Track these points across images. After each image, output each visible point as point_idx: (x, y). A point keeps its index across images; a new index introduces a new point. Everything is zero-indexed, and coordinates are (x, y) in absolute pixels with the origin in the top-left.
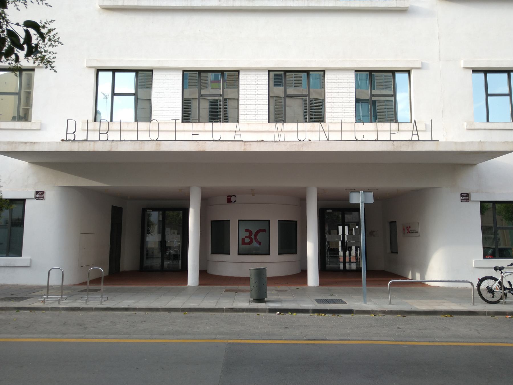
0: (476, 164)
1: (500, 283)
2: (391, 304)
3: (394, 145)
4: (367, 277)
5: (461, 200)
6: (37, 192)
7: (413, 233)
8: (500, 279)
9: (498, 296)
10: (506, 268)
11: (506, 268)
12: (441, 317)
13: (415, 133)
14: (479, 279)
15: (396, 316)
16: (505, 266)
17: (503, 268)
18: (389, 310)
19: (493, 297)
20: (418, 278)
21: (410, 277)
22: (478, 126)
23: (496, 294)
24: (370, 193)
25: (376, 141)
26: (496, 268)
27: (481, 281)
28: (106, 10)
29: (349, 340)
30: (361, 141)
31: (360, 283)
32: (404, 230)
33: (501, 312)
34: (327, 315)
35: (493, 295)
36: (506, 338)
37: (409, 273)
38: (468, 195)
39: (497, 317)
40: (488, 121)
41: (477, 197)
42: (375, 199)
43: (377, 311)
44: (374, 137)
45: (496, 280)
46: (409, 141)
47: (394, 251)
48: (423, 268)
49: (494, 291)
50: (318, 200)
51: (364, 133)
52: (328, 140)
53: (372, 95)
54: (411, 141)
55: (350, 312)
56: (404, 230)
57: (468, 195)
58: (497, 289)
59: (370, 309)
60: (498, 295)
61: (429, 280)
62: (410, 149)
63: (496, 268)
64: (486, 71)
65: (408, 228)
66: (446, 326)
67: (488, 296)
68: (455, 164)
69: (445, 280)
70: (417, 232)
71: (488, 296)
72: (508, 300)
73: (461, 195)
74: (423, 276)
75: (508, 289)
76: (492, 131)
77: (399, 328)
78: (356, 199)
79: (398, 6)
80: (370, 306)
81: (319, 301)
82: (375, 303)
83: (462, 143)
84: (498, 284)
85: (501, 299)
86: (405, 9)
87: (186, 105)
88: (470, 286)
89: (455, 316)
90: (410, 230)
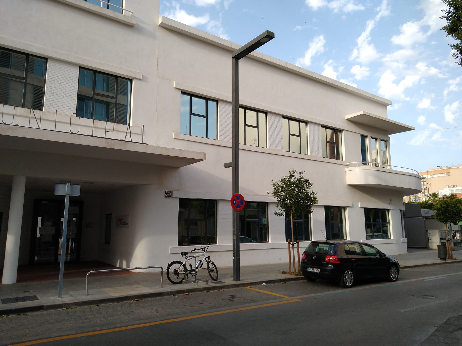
0: (179, 168)
1: (184, 266)
2: (88, 295)
3: (108, 143)
4: (65, 269)
5: (165, 196)
6: (166, 191)
7: (124, 224)
8: (184, 263)
9: (181, 276)
10: (190, 253)
11: (190, 253)
12: (132, 301)
13: (129, 134)
14: (169, 264)
15: (89, 307)
16: (189, 251)
17: (187, 253)
18: (83, 301)
19: (178, 278)
20: (124, 267)
21: (118, 265)
22: (182, 137)
23: (180, 275)
24: (78, 186)
25: (91, 136)
26: (182, 254)
27: (170, 265)
28: (163, 29)
29: (62, 336)
30: (76, 134)
31: (57, 276)
32: (117, 222)
33: (180, 291)
34: (11, 316)
35: (178, 276)
36: (177, 313)
37: (117, 261)
38: (171, 192)
39: (177, 295)
40: (190, 135)
41: (178, 195)
42: (82, 192)
43: (69, 304)
44: (96, 132)
45: (181, 263)
46: (123, 140)
47: (108, 242)
48: (128, 256)
49: (179, 273)
50: (26, 190)
51: (79, 127)
52: (39, 128)
53: (95, 93)
54: (125, 141)
55: (40, 308)
56: (117, 222)
57: (171, 192)
58: (181, 271)
59: (63, 303)
60: (181, 276)
61: (134, 267)
62: (122, 148)
63: (182, 254)
64: (192, 95)
65: (121, 220)
66: (132, 310)
67: (174, 277)
68: (165, 166)
69: (147, 266)
70: (127, 224)
71: (174, 277)
72: (189, 279)
73: (166, 192)
74: (128, 265)
75: (190, 270)
76: (192, 143)
77: (87, 319)
78: (63, 191)
79: (125, 20)
80: (66, 299)
81: (4, 301)
82: (71, 296)
83: (167, 148)
84: (183, 267)
85: (184, 279)
86: (132, 25)
87: (81, 98)
88: (160, 269)
89: (144, 299)
90: (123, 223)
